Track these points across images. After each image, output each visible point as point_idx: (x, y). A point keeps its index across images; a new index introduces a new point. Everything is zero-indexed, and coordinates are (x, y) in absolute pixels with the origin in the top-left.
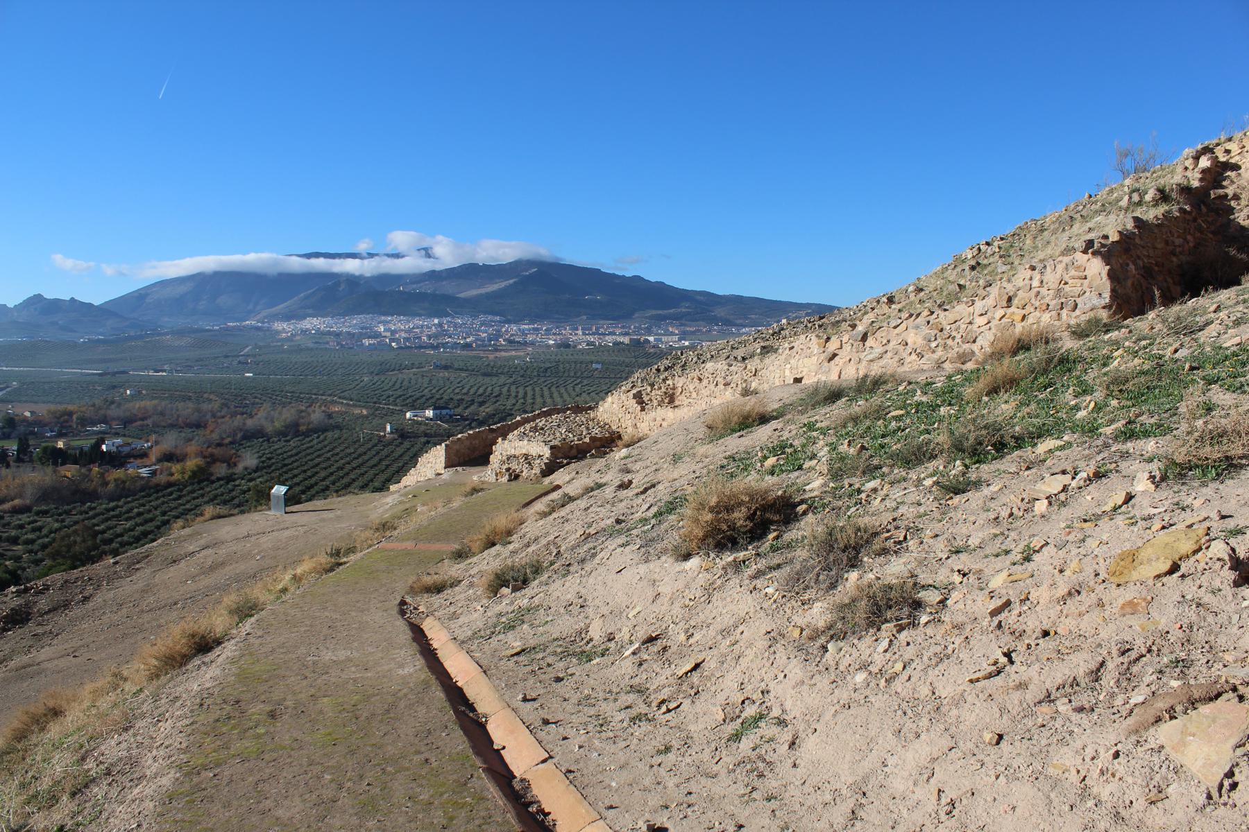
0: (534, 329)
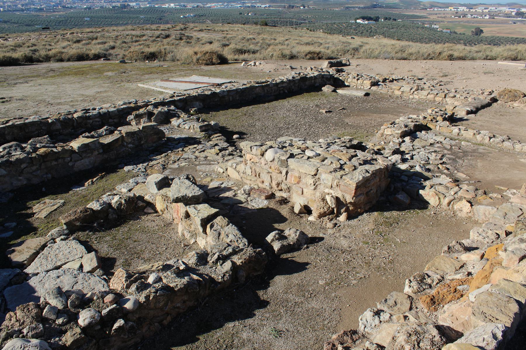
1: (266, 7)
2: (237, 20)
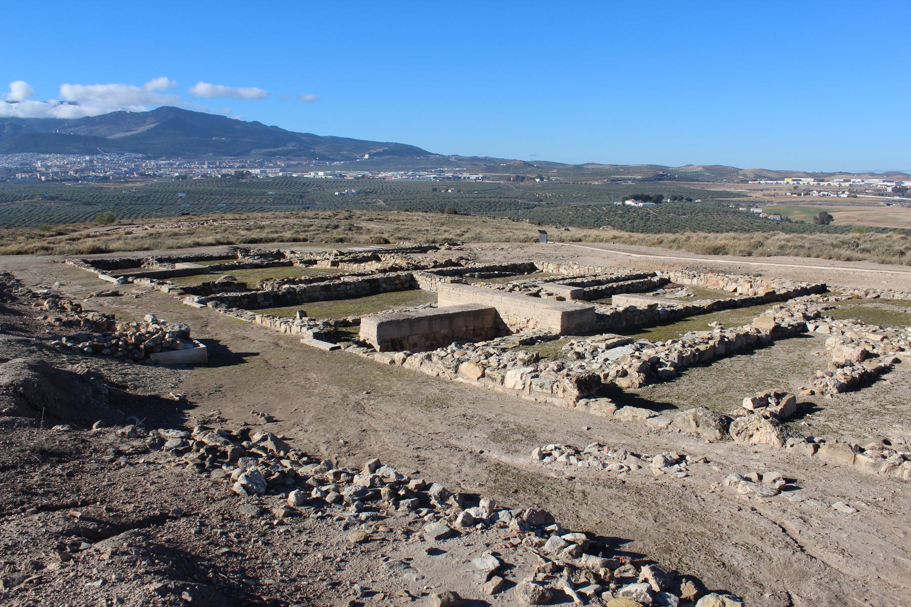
0: (169, 164)
1: (478, 178)
2: (428, 200)
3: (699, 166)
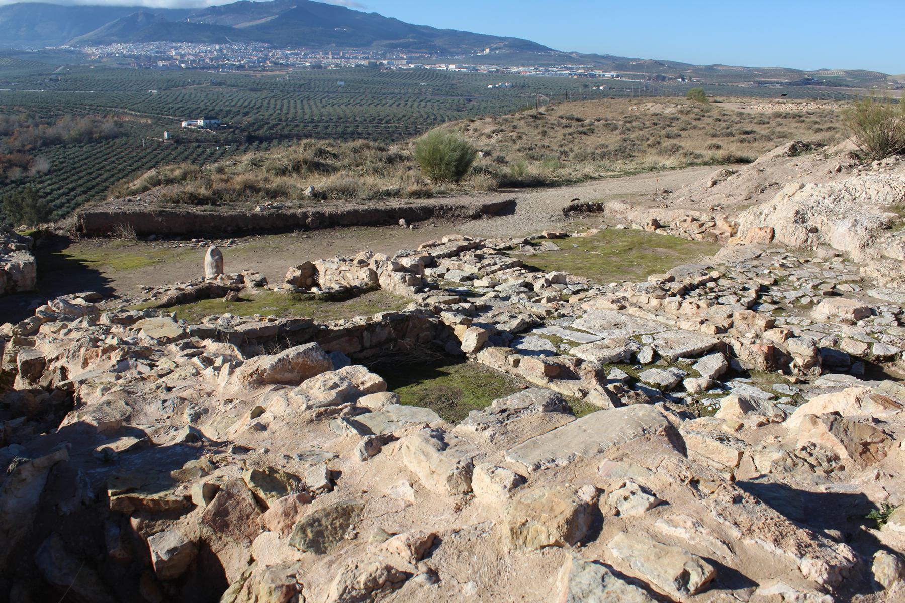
0: (295, 54)
3: (842, 71)
